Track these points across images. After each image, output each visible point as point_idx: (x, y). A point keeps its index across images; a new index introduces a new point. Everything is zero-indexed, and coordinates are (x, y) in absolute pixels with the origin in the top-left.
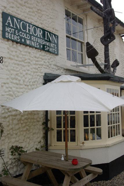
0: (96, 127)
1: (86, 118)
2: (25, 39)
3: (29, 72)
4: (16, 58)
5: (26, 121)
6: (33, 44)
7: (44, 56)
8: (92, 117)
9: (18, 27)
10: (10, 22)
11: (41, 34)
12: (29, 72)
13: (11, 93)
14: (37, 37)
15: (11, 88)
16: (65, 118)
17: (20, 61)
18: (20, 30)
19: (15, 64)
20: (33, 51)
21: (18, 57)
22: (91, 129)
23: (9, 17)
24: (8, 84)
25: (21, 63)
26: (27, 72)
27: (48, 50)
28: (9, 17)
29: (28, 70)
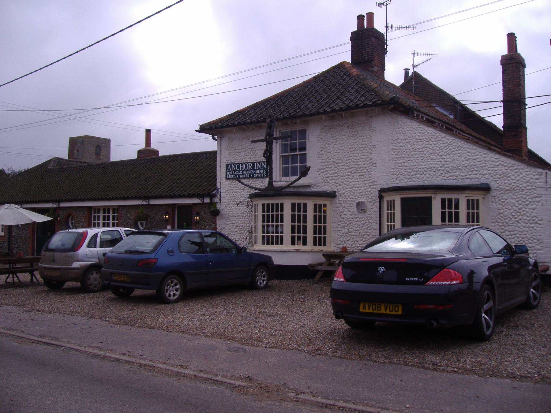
0: (302, 235)
1: (457, 220)
2: (239, 175)
3: (243, 195)
4: (235, 188)
5: (241, 227)
6: (244, 176)
7: (256, 181)
8: (473, 222)
9: (235, 169)
10: (230, 168)
11: (251, 167)
12: (243, 195)
13: (232, 210)
14: (248, 170)
15: (231, 207)
16: (450, 220)
17: (237, 190)
18: (236, 170)
19: (234, 192)
20: (246, 181)
21: (236, 187)
22: (298, 236)
23: (52, 219)
24: (230, 205)
25: (237, 191)
26: (242, 195)
27: (257, 176)
28: (52, 219)
29: (243, 194)
